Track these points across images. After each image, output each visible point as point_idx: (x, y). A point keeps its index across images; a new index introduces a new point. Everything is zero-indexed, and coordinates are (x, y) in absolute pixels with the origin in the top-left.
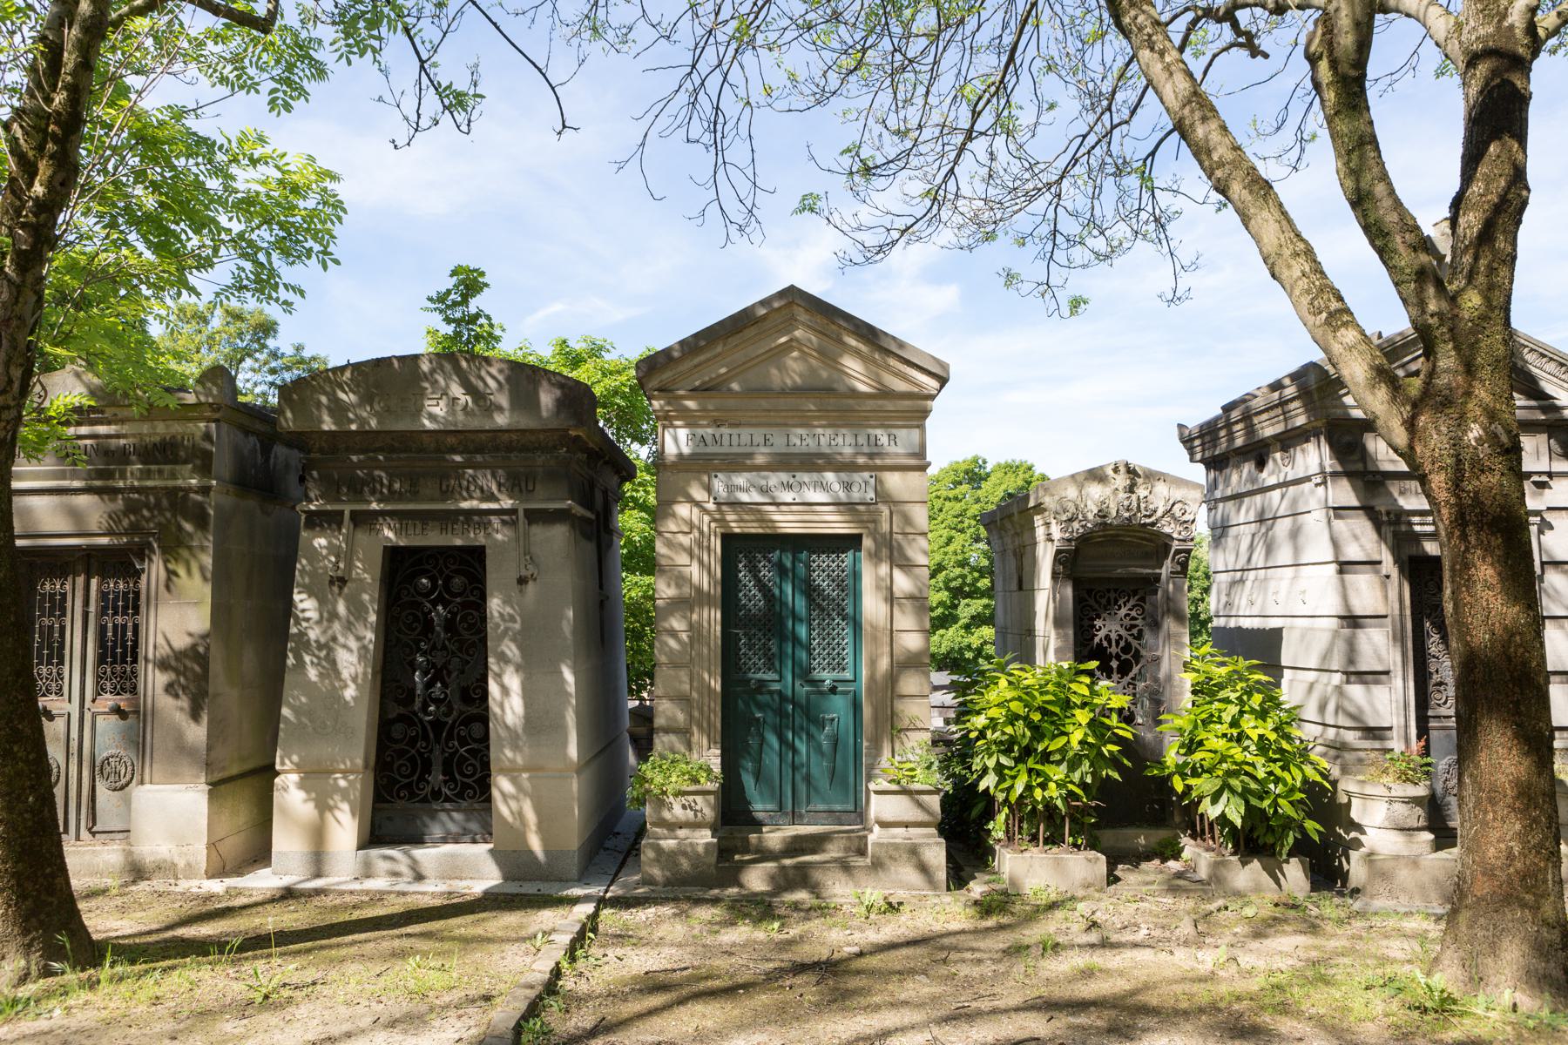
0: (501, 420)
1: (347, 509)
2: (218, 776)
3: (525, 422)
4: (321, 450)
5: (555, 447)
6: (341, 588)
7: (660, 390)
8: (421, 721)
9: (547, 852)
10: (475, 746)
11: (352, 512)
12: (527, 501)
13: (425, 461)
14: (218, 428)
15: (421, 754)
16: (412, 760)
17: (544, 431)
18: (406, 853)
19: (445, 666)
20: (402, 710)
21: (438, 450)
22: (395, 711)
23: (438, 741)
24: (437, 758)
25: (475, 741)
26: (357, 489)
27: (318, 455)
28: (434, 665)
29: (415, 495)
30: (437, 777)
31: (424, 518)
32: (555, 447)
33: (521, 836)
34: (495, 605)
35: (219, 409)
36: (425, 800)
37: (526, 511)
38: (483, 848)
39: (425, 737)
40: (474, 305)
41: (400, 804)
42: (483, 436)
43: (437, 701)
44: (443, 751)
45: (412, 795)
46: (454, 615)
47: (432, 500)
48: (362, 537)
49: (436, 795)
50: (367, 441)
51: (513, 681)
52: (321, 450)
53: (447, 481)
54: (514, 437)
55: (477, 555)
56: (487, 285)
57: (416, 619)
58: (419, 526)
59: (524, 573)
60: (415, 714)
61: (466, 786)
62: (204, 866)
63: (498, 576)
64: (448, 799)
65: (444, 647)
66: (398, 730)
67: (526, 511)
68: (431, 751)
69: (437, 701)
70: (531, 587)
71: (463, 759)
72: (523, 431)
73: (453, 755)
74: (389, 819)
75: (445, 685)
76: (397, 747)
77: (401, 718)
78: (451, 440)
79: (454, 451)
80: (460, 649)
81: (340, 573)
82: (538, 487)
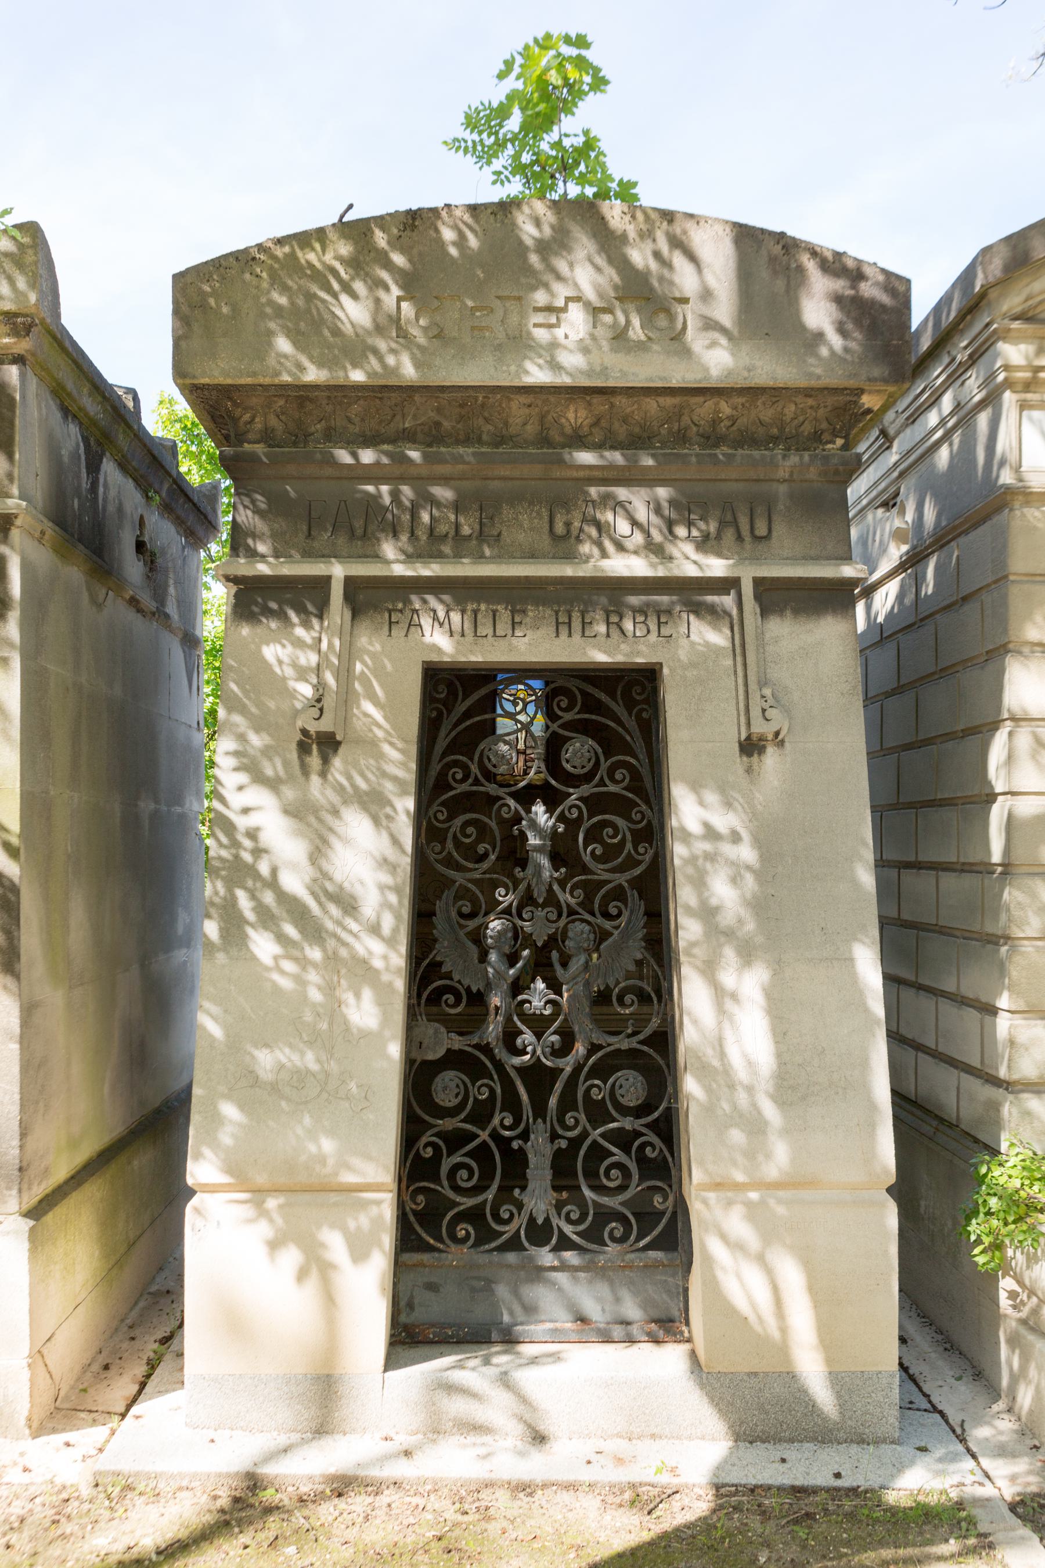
0: (716, 360)
1: (338, 571)
2: (39, 1190)
3: (769, 368)
4: (267, 437)
5: (817, 437)
6: (326, 761)
7: (1023, 317)
8: (499, 1066)
9: (836, 1379)
10: (627, 1123)
11: (349, 581)
12: (755, 559)
13: (505, 459)
14: (22, 376)
15: (503, 1143)
16: (482, 1154)
17: (808, 392)
18: (505, 1380)
19: (553, 942)
20: (457, 1043)
21: (544, 440)
22: (442, 1042)
23: (540, 1110)
24: (539, 1151)
25: (624, 1111)
26: (360, 525)
27: (259, 449)
28: (528, 940)
29: (486, 538)
30: (538, 1199)
31: (517, 598)
32: (817, 437)
33: (783, 1350)
34: (689, 810)
35: (28, 329)
36: (514, 1244)
37: (758, 582)
38: (671, 1358)
39: (512, 1104)
40: (570, 128)
41: (457, 1255)
42: (651, 405)
43: (539, 1025)
44: (554, 1136)
45: (485, 1236)
46: (572, 826)
47: (532, 555)
48: (371, 642)
49: (540, 1233)
50: (385, 411)
51: (751, 983)
52: (267, 437)
53: (566, 511)
54: (726, 409)
55: (640, 686)
56: (573, 114)
57: (483, 831)
58: (504, 615)
59: (759, 727)
60: (487, 1049)
61: (604, 1216)
62: (23, 1408)
63: (693, 732)
64: (564, 1244)
65: (551, 900)
66: (447, 1088)
67: (758, 582)
68: (525, 1136)
69: (539, 1025)
70: (771, 758)
71: (597, 1153)
72: (753, 393)
73: (575, 1144)
74: (432, 1287)
75: (554, 986)
76: (448, 1124)
77: (453, 1060)
78: (575, 416)
79: (579, 441)
80: (587, 904)
81: (325, 725)
82: (780, 529)
